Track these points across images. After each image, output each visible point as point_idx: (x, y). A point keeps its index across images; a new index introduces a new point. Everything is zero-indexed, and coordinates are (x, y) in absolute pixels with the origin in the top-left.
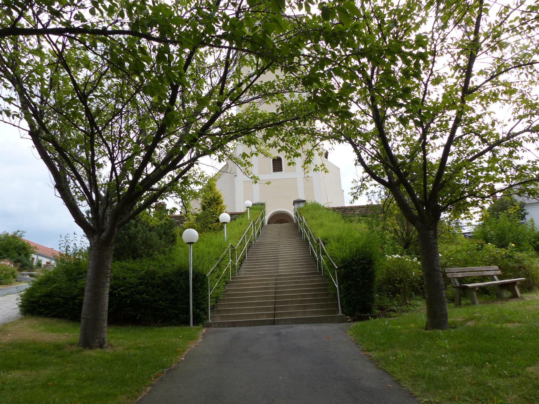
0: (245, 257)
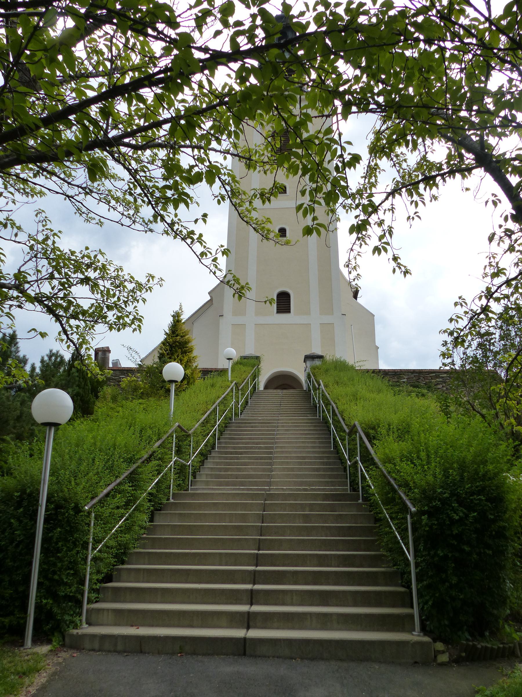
0: (213, 447)
